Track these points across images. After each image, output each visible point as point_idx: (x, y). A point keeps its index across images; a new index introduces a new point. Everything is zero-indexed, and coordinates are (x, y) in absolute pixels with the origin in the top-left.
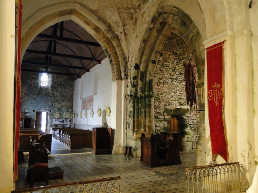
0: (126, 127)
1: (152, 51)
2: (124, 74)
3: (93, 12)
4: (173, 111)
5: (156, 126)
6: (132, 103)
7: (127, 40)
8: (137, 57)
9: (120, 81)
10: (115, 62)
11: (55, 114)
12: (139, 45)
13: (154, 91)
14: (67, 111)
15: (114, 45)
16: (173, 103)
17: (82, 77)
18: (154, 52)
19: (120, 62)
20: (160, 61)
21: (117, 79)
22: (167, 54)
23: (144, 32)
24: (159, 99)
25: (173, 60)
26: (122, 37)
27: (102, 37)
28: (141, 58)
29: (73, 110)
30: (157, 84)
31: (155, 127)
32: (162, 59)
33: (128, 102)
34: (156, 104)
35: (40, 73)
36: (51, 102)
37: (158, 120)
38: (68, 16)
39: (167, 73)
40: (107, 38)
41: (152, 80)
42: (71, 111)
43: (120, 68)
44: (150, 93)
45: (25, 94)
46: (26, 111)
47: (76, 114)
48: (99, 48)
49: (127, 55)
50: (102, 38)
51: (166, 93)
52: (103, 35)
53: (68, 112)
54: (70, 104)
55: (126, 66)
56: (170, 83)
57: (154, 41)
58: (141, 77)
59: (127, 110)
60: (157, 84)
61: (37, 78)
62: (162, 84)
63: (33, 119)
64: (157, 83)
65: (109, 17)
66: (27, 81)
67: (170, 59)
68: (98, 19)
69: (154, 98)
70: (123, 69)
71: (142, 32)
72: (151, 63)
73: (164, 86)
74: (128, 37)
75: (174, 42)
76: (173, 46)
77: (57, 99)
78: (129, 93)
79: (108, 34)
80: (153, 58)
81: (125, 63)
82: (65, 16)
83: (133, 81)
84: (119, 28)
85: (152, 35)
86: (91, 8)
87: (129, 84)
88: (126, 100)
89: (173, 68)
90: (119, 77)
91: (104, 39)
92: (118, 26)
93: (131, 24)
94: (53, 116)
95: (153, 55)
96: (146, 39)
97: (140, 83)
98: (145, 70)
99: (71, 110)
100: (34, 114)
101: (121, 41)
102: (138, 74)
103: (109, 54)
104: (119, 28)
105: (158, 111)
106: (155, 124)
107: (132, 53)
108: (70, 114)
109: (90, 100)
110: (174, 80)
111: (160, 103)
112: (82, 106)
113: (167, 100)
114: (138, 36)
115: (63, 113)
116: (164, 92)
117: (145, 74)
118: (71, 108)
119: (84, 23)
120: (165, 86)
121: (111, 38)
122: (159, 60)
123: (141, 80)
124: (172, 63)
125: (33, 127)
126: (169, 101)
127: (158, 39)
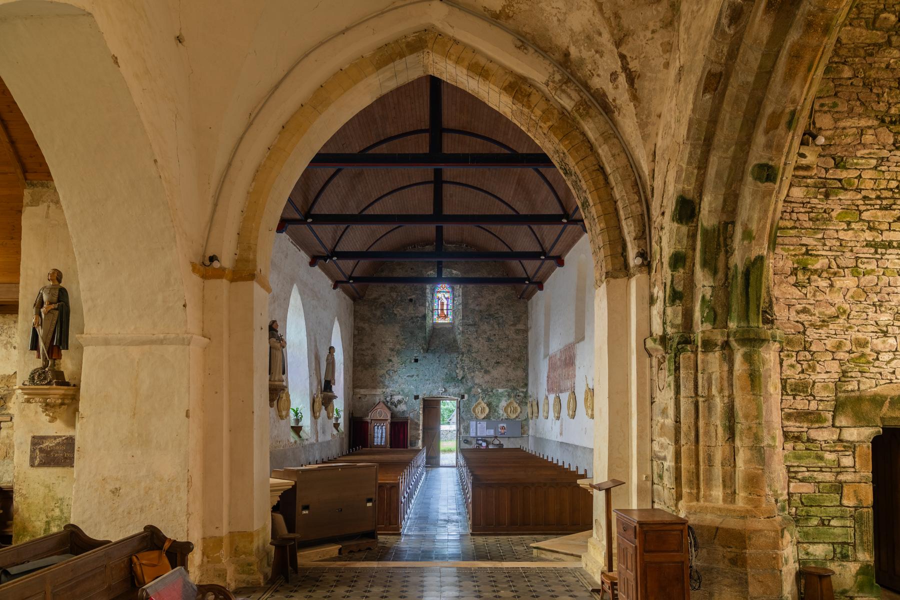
0: (649, 473)
1: (750, 123)
2: (636, 251)
3: (495, 18)
4: (887, 403)
5: (792, 475)
6: (669, 371)
7: (640, 103)
8: (684, 166)
9: (621, 281)
10: (599, 207)
11: (476, 406)
12: (691, 106)
13: (780, 313)
14: (509, 396)
15: (591, 135)
16: (889, 362)
17: (545, 284)
18: (763, 124)
19: (619, 203)
20: (807, 168)
21: (607, 273)
22: (844, 128)
23: (709, 37)
24: (805, 349)
25: (885, 153)
26: (619, 94)
27: (538, 112)
28: (702, 165)
29: (530, 393)
30: (792, 280)
31: (789, 482)
32: (820, 156)
33: (655, 370)
34: (788, 372)
35: (428, 287)
36: (463, 368)
37: (800, 446)
38: (411, 58)
39: (849, 223)
40: (563, 112)
41: (760, 259)
42: (521, 394)
43: (619, 228)
44: (753, 324)
45: (392, 350)
46: (395, 397)
47: (535, 403)
48: (553, 169)
49: (645, 168)
50: (541, 118)
51: (845, 317)
52: (544, 106)
53: (512, 399)
54: (519, 373)
55: (642, 215)
56: (869, 267)
57: (760, 67)
58: (704, 251)
59: (652, 403)
60: (792, 280)
61: (420, 300)
62: (825, 275)
63: (416, 421)
64: (794, 272)
65: (559, 20)
66: (395, 312)
67: (867, 151)
68: (519, 44)
69: (777, 345)
70: (632, 228)
71: (701, 42)
72: (749, 179)
73: (832, 286)
74: (645, 86)
75: (888, 66)
76: (881, 87)
77: (478, 359)
78: (657, 330)
79: (563, 96)
80: (758, 154)
81: (641, 205)
82: (399, 64)
83: (672, 276)
84: (601, 57)
85: (747, 40)
86: (485, 5)
87: (658, 292)
88: (648, 360)
89: (888, 194)
90: (618, 267)
91: (549, 120)
92: (597, 52)
93: (651, 25)
94: (470, 412)
95: (760, 139)
96: (717, 69)
97: (704, 283)
98: (724, 218)
99: (522, 392)
100: (418, 406)
101: (616, 113)
102: (694, 241)
103: (573, 177)
104: (601, 57)
105: (800, 404)
106: (788, 467)
107: (665, 155)
108: (519, 405)
109: (566, 359)
110: (890, 251)
111: (814, 370)
112: (548, 381)
113: (849, 352)
114: (686, 68)
115: (500, 401)
116: (832, 311)
117: (725, 239)
118: (522, 387)
119: (471, 74)
120: (838, 283)
121: (576, 111)
122: (804, 162)
123: (705, 264)
124: (875, 168)
125: (414, 443)
126: (863, 355)
127: (779, 52)
